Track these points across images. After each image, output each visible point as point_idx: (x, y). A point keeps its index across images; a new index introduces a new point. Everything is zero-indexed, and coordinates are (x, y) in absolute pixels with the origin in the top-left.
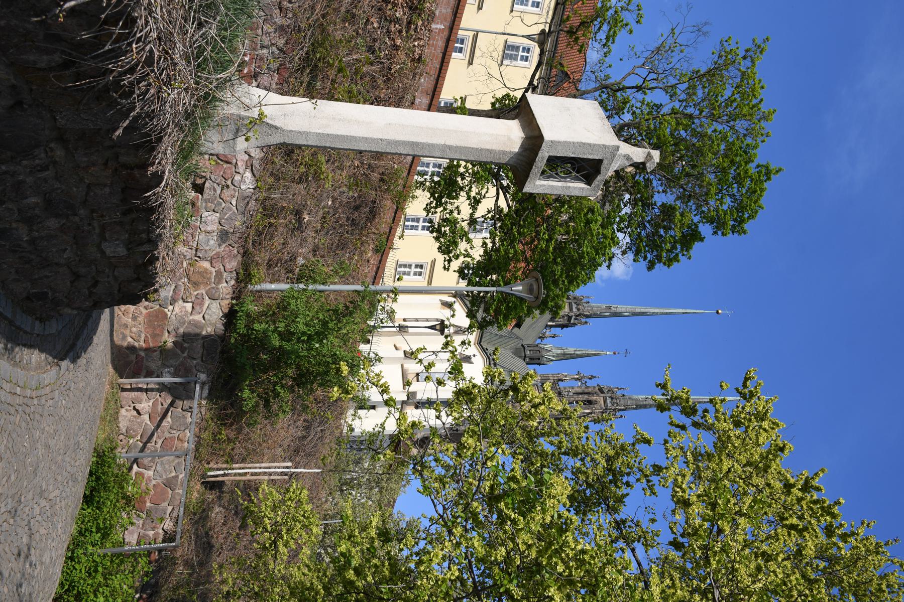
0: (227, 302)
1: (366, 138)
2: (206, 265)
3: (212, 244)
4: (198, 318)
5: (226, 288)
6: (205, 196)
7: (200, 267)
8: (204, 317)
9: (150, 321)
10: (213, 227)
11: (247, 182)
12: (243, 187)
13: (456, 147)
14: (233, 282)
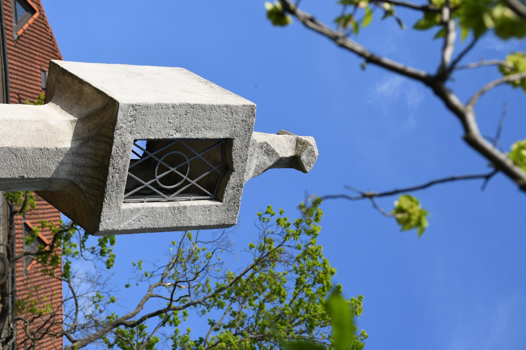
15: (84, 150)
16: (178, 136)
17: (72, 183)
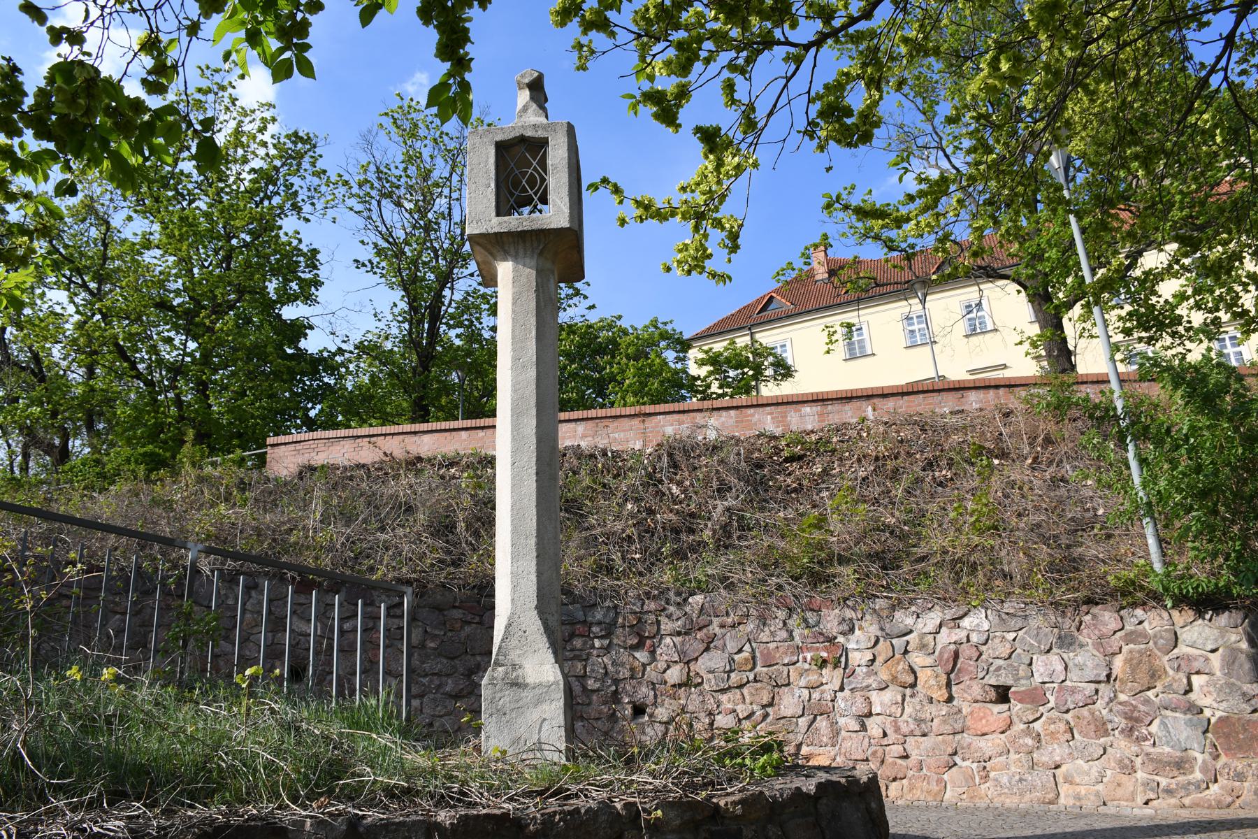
0: (1175, 613)
1: (513, 486)
2: (1118, 663)
3: (1087, 660)
4: (1216, 660)
5: (1153, 621)
6: (1009, 682)
7: (1124, 672)
8: (1213, 651)
9: (1240, 748)
10: (1055, 662)
11: (977, 622)
12: (986, 626)
13: (514, 350)
14: (1139, 612)
15: (512, 252)
16: (493, 185)
17: (541, 254)
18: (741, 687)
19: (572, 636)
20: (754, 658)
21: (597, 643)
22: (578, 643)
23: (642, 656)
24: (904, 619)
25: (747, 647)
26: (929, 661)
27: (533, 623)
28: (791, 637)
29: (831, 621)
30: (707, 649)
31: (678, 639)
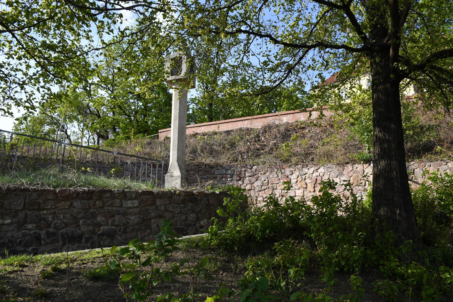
0: (364, 165)
18: (264, 190)
19: (222, 177)
20: (268, 182)
21: (229, 179)
22: (224, 179)
23: (240, 182)
24: (305, 170)
25: (267, 179)
26: (310, 181)
27: (176, 164)
28: (278, 176)
29: (288, 171)
30: (257, 180)
31: (249, 178)
